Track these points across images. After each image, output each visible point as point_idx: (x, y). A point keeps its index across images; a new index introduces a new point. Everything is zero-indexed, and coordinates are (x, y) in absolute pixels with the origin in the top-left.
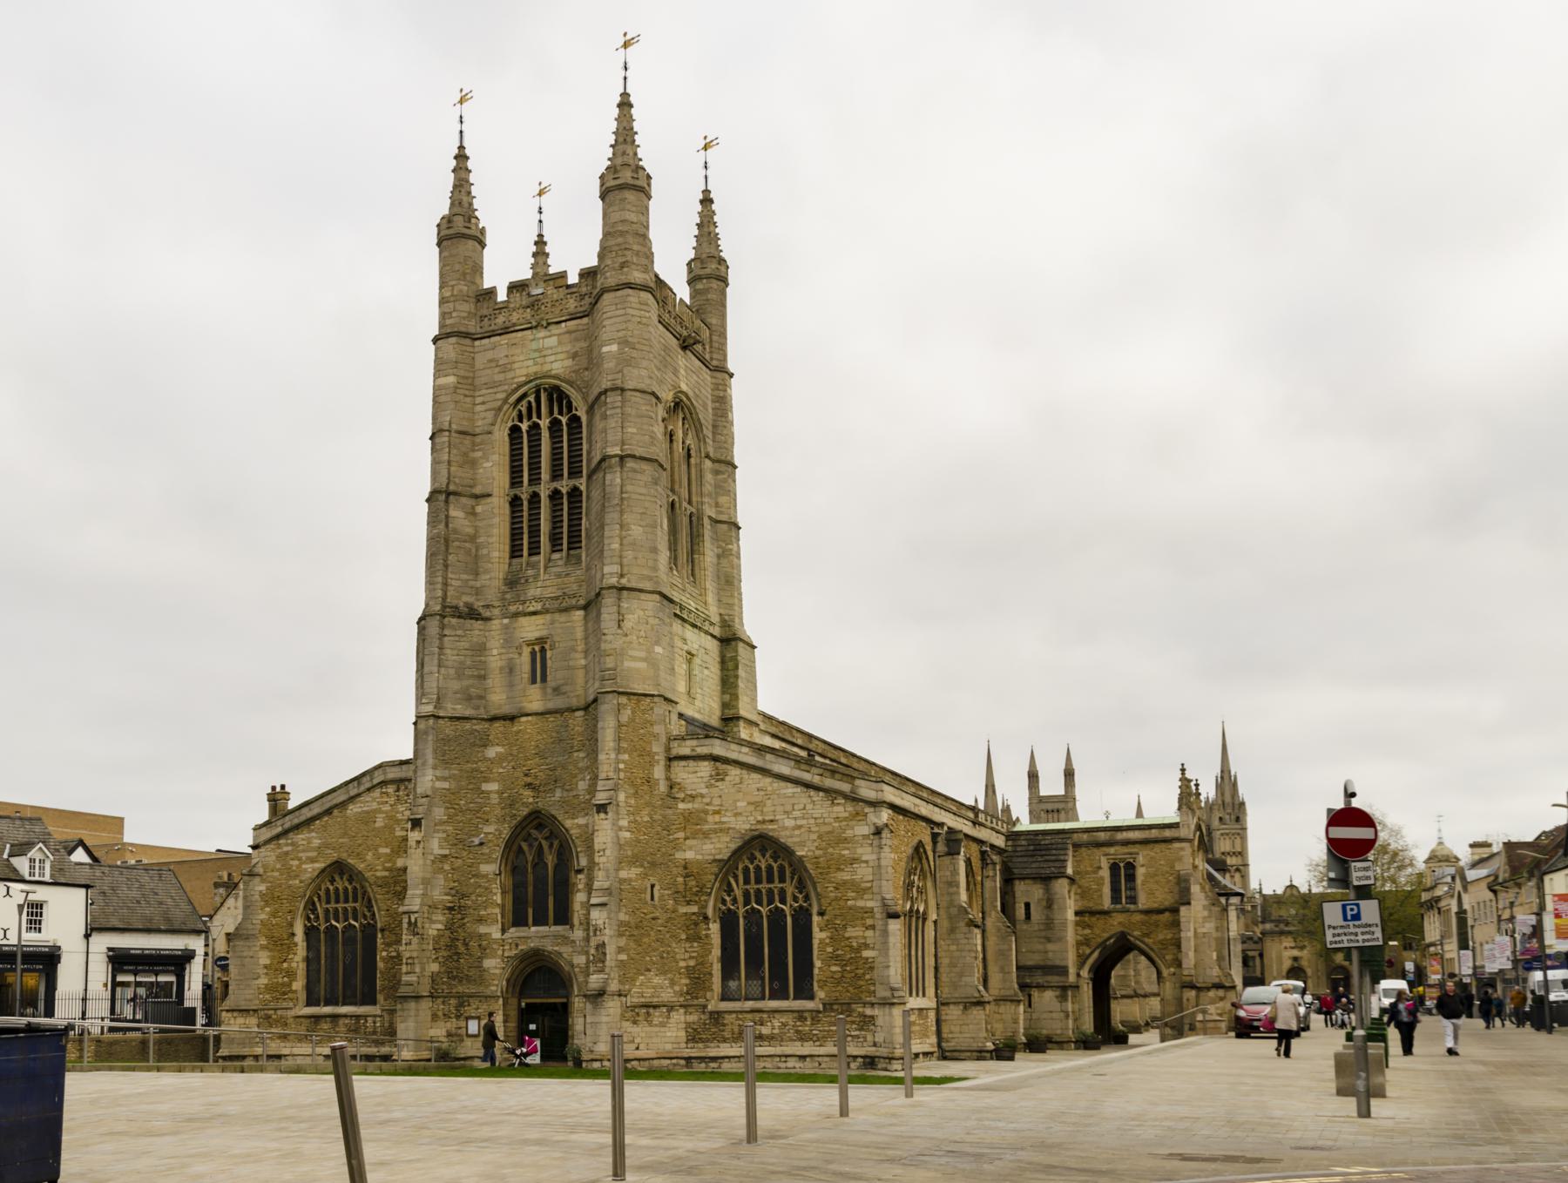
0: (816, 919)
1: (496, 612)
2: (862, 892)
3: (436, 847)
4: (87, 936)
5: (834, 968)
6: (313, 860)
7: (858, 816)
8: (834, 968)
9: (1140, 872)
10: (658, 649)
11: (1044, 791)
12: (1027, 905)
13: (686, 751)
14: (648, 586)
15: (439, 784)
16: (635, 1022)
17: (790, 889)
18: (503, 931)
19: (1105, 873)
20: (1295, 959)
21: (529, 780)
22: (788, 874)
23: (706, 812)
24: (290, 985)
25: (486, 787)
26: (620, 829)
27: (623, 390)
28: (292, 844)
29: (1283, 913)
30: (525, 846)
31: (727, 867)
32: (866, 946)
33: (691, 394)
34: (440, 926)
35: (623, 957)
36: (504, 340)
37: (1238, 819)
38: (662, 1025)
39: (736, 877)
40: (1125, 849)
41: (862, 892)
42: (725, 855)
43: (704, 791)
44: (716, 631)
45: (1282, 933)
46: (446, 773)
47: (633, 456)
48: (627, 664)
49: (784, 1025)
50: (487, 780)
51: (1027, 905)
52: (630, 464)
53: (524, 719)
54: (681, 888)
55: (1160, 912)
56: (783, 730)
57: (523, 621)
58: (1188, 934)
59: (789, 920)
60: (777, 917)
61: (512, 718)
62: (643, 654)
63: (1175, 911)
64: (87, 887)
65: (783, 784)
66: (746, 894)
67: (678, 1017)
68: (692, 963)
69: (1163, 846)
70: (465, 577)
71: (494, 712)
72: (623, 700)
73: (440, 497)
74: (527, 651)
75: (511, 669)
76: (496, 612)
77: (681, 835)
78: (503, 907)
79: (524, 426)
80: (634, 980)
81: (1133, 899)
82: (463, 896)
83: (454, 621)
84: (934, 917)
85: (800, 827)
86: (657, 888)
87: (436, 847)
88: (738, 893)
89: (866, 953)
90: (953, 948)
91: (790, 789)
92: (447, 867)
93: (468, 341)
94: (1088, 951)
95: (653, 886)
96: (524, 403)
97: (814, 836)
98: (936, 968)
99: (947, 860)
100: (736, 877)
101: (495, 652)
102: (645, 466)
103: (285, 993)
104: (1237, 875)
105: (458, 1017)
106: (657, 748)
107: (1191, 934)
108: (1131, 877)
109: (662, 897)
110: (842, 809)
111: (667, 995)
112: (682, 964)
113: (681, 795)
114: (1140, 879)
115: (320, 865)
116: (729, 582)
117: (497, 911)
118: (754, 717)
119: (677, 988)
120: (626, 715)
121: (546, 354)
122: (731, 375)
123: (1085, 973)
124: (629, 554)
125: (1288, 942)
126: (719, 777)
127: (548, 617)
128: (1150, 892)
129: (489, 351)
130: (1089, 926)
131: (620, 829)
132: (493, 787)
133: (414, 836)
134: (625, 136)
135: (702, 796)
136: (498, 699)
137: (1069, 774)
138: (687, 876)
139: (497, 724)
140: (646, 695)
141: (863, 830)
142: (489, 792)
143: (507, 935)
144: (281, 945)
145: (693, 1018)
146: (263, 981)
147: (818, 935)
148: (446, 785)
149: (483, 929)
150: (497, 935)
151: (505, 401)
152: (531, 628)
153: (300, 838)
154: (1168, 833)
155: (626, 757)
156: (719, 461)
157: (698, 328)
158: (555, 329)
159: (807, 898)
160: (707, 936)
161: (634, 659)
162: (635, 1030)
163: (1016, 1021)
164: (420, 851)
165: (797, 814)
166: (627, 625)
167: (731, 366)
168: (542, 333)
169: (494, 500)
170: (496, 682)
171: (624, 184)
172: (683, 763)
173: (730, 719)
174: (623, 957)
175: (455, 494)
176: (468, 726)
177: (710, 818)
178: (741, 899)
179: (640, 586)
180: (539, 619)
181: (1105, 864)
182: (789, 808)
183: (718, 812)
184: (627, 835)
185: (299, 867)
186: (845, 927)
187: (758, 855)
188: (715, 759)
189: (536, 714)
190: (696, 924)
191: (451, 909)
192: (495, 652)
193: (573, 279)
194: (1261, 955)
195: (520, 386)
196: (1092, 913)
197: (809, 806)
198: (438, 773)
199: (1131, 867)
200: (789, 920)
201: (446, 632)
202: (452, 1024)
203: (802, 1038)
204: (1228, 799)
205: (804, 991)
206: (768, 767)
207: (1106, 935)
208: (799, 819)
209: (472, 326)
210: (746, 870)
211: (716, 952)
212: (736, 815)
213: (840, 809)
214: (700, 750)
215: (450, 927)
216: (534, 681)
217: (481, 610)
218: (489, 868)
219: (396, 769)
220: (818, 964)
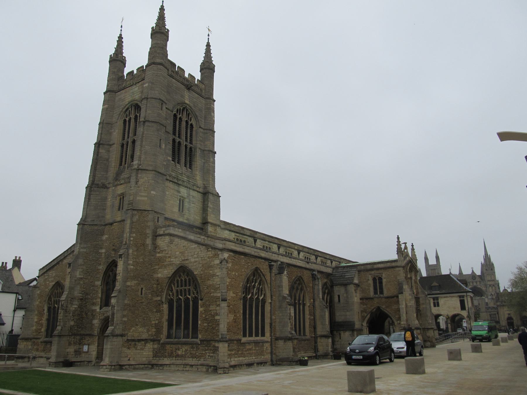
0: (200, 302)
1: (111, 185)
2: (216, 289)
3: (78, 274)
4: (15, 311)
5: (205, 324)
6: (52, 281)
7: (216, 256)
8: (205, 324)
9: (384, 281)
10: (152, 192)
11: (430, 263)
12: (339, 296)
13: (162, 233)
14: (151, 168)
15: (82, 250)
16: (129, 348)
17: (192, 288)
18: (101, 308)
19: (371, 282)
20: (509, 314)
21: (114, 247)
22: (192, 282)
23: (166, 257)
24: (41, 329)
25: (100, 251)
26: (129, 265)
27: (147, 98)
28: (48, 276)
29: (503, 299)
30: (111, 273)
31: (172, 279)
32: (217, 314)
33: (191, 105)
34: (76, 306)
35: (125, 319)
36: (123, 91)
37: (492, 269)
38: (142, 349)
39: (174, 284)
40: (378, 272)
41: (216, 289)
42: (169, 276)
43: (166, 248)
44: (201, 190)
45: (503, 306)
46: (85, 246)
47: (149, 121)
48: (138, 198)
49: (186, 350)
50: (101, 248)
51: (339, 296)
52: (147, 124)
53: (115, 224)
54: (155, 289)
55: (393, 297)
56: (240, 231)
57: (119, 187)
58: (403, 306)
59: (191, 303)
60: (187, 300)
61: (111, 224)
62: (146, 194)
63: (398, 297)
64: (17, 293)
65: (191, 244)
66: (177, 291)
67: (150, 346)
68: (157, 322)
69: (392, 269)
70: (103, 173)
71: (107, 222)
72: (135, 212)
73: (98, 145)
74: (118, 198)
75: (113, 206)
76: (111, 185)
77: (157, 267)
78: (101, 299)
79: (127, 119)
80: (130, 329)
81: (382, 292)
82: (87, 294)
83: (96, 189)
84: (270, 301)
85: (196, 262)
86: (144, 289)
87: (78, 274)
88: (174, 291)
89: (217, 317)
90: (281, 314)
91: (194, 246)
92: (81, 282)
93: (114, 93)
94: (366, 315)
95: (142, 289)
96: (128, 111)
97: (200, 265)
98: (271, 324)
99: (278, 276)
100: (174, 284)
101: (109, 200)
102: (153, 124)
103: (39, 333)
104: (494, 287)
105: (80, 344)
106: (149, 232)
107: (404, 306)
108: (381, 283)
109: (146, 293)
110: (210, 254)
111: (145, 336)
112: (153, 322)
113: (159, 251)
114: (384, 284)
115: (54, 283)
116: (209, 171)
117: (99, 300)
118: (218, 223)
119: (150, 333)
120: (135, 219)
121: (133, 94)
122: (214, 101)
123: (365, 324)
124: (143, 157)
125: (506, 309)
126: (171, 242)
127: (125, 185)
128: (388, 290)
129: (122, 95)
130: (366, 305)
131: (129, 265)
132: (103, 251)
133: (69, 270)
134: (161, 18)
135: (165, 250)
136: (109, 218)
137: (437, 258)
138: (158, 284)
139: (107, 227)
140: (145, 210)
141: (217, 262)
142: (102, 253)
143: (102, 310)
144: (41, 314)
145: (156, 346)
146: (34, 328)
147: (201, 309)
148: (85, 250)
149: (94, 308)
150: (98, 310)
151: (122, 111)
152: (120, 190)
153: (50, 273)
154: (394, 264)
155: (134, 235)
156: (207, 129)
157: (202, 88)
158: (138, 85)
159: (197, 292)
160: (163, 310)
161: (142, 196)
162: (128, 351)
163: (327, 346)
164: (69, 276)
165: (195, 256)
166: (140, 183)
167: (214, 98)
168: (134, 87)
169: (115, 145)
170: (108, 211)
171: (160, 33)
172: (160, 237)
173: (205, 223)
174: (125, 319)
175: (102, 144)
176: (96, 228)
177: (167, 260)
178: (175, 294)
179: (147, 168)
180: (122, 186)
181: (370, 278)
182: (193, 254)
183: (169, 257)
184: (132, 267)
185: (49, 284)
186: (209, 305)
187: (182, 274)
188: (170, 235)
189: (118, 222)
190: (159, 305)
191: (81, 299)
192: (109, 200)
193: (135, 72)
194: (498, 313)
195: (126, 106)
196: (367, 299)
197: (200, 253)
198: (82, 246)
199: (380, 279)
200: (191, 303)
201: (92, 193)
202: (77, 347)
203: (193, 356)
204: (488, 263)
205: (195, 336)
206: (187, 237)
207: (373, 308)
208: (194, 256)
209: (116, 88)
210: (178, 281)
211: (166, 317)
212: (176, 258)
213: (210, 253)
214: (167, 232)
215: (80, 306)
216: (119, 210)
217: (107, 185)
218: (99, 283)
219: (250, 232)
220: (199, 322)
